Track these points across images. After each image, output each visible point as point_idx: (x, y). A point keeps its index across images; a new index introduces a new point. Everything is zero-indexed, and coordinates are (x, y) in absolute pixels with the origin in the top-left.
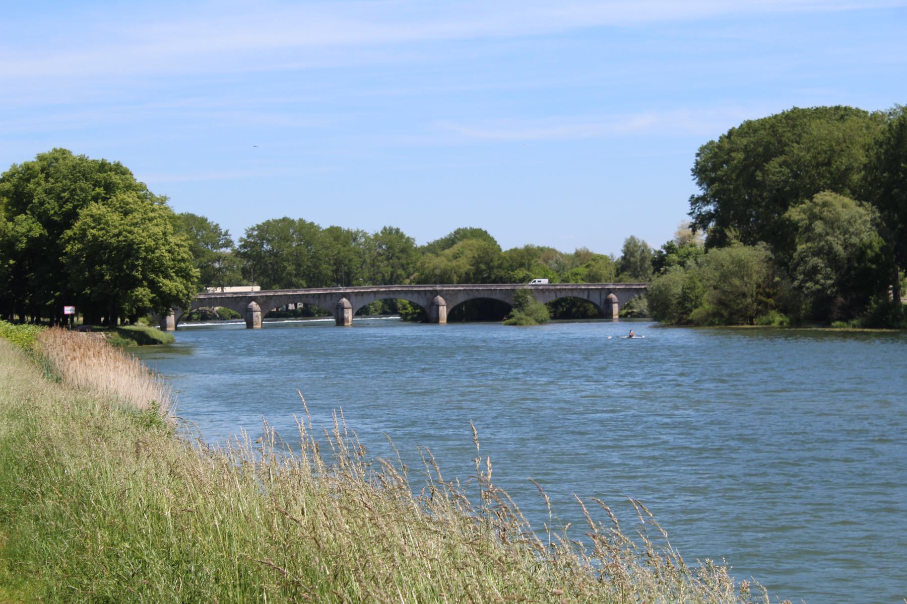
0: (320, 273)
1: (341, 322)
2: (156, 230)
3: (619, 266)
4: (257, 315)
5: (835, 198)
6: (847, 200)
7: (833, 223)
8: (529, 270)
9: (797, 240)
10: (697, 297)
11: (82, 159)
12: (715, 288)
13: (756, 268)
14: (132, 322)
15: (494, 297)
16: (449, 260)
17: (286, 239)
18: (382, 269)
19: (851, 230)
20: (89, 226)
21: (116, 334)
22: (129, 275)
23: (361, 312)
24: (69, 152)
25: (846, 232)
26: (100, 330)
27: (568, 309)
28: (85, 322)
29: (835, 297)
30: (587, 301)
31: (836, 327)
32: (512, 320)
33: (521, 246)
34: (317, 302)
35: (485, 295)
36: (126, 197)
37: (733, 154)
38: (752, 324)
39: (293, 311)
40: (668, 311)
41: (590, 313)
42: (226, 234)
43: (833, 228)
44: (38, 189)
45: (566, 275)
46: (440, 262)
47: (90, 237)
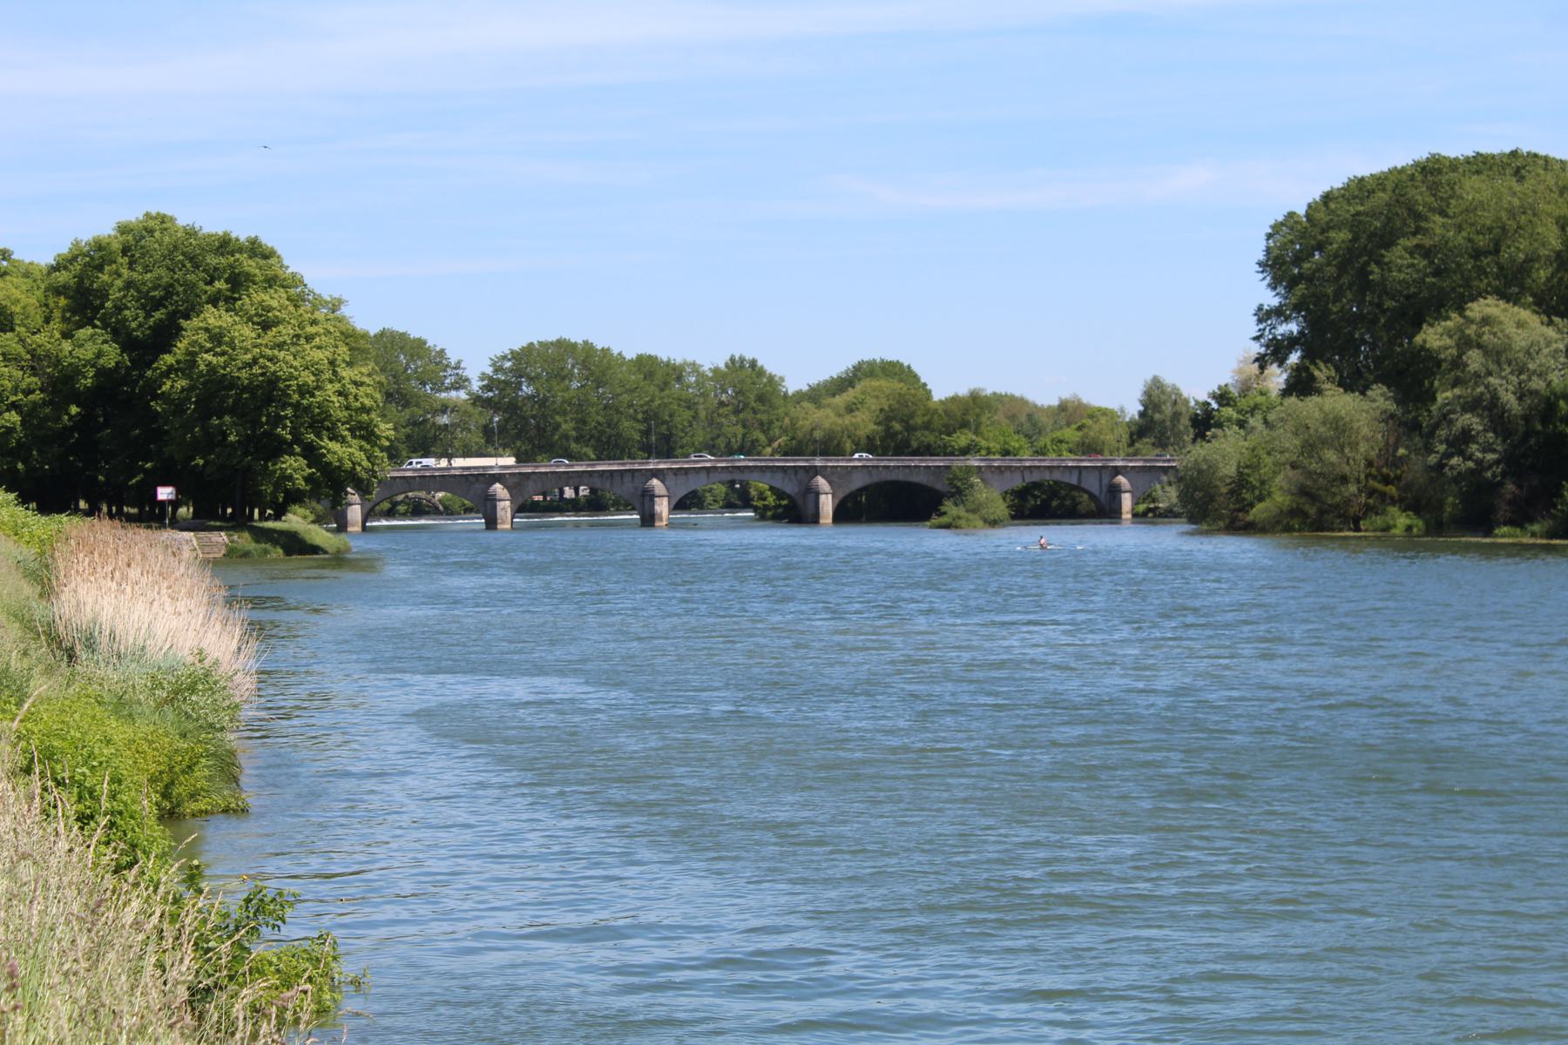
0: (619, 435)
1: (649, 520)
2: (318, 355)
3: (1134, 428)
4: (504, 508)
5: (1505, 310)
6: (1525, 314)
7: (1499, 353)
8: (976, 433)
9: (1436, 383)
10: (1263, 482)
11: (191, 233)
12: (1294, 466)
13: (1365, 431)
14: (278, 516)
15: (915, 479)
16: (840, 416)
17: (562, 376)
18: (726, 429)
19: (1531, 366)
20: (201, 347)
21: (246, 535)
22: (270, 435)
23: (687, 503)
24: (172, 219)
25: (1521, 370)
26: (220, 529)
27: (1042, 502)
28: (196, 515)
29: (1500, 484)
30: (1078, 488)
31: (1503, 536)
32: (944, 520)
33: (963, 391)
34: (608, 486)
35: (900, 476)
36: (266, 297)
37: (1332, 234)
38: (1358, 529)
39: (571, 500)
40: (1213, 506)
41: (1082, 509)
42: (457, 368)
43: (1499, 363)
44: (113, 281)
45: (1041, 444)
46: (825, 418)
47: (202, 367)
